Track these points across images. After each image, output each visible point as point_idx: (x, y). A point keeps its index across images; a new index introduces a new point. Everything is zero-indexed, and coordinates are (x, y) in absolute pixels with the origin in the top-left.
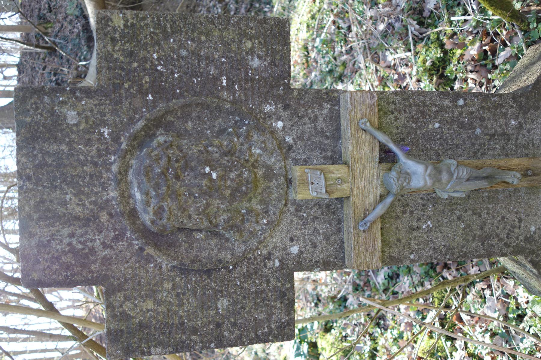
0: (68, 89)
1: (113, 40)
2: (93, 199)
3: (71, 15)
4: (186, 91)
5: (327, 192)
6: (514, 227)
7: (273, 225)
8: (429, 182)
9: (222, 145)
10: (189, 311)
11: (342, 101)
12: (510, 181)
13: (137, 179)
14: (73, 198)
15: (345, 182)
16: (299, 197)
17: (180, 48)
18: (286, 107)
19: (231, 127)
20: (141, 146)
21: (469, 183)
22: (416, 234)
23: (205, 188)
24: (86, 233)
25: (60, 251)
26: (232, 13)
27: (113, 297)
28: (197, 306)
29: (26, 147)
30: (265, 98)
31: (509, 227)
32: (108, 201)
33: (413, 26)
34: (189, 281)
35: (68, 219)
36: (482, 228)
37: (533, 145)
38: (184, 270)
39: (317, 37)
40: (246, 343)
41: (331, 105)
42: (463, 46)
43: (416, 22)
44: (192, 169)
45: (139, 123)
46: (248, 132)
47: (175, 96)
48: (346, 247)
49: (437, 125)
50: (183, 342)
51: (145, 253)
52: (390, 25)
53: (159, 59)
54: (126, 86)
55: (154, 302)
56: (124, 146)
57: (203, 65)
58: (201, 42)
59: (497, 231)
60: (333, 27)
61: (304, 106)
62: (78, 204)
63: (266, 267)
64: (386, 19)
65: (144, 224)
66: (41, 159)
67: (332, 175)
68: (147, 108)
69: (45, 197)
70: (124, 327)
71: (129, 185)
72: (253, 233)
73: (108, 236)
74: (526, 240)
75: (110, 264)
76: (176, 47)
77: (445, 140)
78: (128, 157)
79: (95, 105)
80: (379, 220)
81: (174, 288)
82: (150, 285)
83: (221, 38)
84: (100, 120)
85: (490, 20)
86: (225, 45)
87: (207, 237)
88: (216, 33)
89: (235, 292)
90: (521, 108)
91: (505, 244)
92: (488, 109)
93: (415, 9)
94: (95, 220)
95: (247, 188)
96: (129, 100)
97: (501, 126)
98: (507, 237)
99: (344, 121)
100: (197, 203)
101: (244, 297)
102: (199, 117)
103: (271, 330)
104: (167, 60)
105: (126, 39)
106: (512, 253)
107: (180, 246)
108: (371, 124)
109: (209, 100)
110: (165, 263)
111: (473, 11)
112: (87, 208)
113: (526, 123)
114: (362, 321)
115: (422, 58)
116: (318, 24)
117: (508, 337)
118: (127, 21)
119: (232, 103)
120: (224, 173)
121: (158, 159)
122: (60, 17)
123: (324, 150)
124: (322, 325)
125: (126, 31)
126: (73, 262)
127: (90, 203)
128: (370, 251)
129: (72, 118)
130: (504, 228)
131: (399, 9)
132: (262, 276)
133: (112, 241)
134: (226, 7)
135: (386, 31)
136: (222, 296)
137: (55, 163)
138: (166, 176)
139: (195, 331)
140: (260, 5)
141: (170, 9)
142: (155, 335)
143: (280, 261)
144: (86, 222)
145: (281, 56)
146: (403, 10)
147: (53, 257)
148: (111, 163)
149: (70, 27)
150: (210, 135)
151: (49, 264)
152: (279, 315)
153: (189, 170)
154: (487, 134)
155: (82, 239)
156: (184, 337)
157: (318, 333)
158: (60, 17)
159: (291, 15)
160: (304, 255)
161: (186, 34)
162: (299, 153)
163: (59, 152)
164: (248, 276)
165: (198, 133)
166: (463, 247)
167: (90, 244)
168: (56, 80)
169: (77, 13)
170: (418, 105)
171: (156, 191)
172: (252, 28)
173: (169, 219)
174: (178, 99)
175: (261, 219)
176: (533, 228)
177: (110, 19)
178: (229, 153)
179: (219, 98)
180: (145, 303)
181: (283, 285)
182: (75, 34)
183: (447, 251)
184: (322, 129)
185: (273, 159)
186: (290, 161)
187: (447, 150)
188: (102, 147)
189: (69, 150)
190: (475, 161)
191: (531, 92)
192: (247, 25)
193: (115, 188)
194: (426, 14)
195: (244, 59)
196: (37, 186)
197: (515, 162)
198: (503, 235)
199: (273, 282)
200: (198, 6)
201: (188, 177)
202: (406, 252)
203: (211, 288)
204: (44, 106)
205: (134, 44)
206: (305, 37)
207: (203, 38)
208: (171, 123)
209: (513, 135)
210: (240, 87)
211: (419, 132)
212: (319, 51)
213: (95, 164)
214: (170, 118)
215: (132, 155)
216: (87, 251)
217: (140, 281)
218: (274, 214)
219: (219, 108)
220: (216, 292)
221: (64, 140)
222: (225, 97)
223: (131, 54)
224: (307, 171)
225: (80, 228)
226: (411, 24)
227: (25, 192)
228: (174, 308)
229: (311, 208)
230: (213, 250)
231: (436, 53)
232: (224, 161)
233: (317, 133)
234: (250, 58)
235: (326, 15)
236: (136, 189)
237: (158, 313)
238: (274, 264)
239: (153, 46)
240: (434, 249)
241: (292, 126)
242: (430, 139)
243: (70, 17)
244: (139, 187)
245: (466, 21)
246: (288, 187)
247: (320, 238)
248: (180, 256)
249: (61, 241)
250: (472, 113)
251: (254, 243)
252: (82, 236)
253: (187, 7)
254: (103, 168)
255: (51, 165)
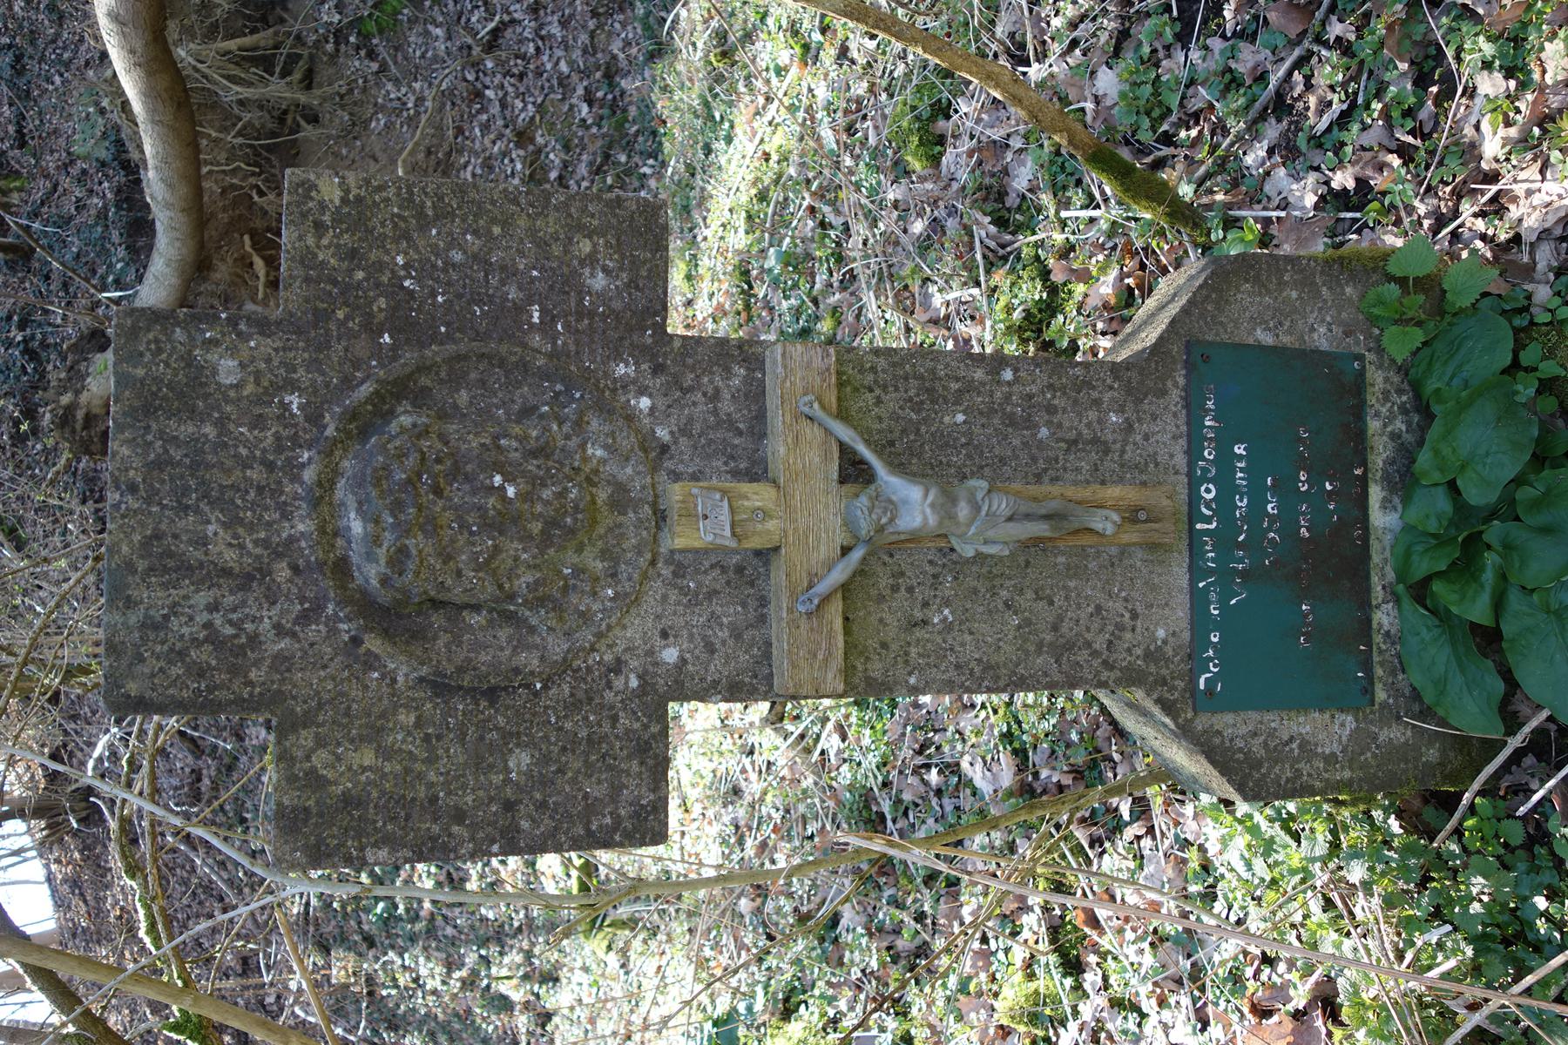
0: (223, 316)
1: (319, 227)
2: (262, 535)
3: (85, 158)
4: (459, 330)
5: (734, 534)
6: (1120, 627)
7: (628, 602)
8: (932, 520)
9: (526, 437)
10: (448, 773)
11: (768, 360)
12: (1098, 526)
13: (355, 494)
14: (221, 532)
15: (771, 517)
16: (680, 543)
17: (450, 246)
18: (658, 369)
19: (547, 404)
20: (364, 434)
21: (1011, 524)
22: (919, 633)
23: (492, 512)
24: (244, 603)
25: (187, 637)
26: (553, 175)
27: (292, 738)
28: (466, 763)
29: (132, 426)
30: (616, 350)
31: (1111, 628)
32: (292, 540)
33: (984, 227)
34: (450, 712)
35: (209, 573)
36: (1055, 628)
37: (1157, 465)
38: (440, 687)
39: (771, 245)
40: (566, 847)
41: (748, 369)
42: (1085, 276)
43: (988, 219)
44: (468, 478)
45: (363, 388)
46: (581, 414)
47: (435, 338)
48: (775, 652)
49: (960, 418)
50: (434, 839)
51: (362, 650)
52: (936, 225)
53: (406, 266)
54: (340, 314)
55: (377, 751)
56: (330, 431)
57: (494, 282)
58: (490, 237)
59: (1088, 636)
60: (811, 223)
61: (693, 369)
62: (230, 545)
63: (610, 688)
64: (928, 210)
65: (364, 592)
66: (160, 451)
67: (746, 503)
68: (379, 359)
69: (163, 527)
70: (311, 803)
71: (337, 509)
72: (585, 616)
73: (288, 611)
74: (1148, 656)
75: (288, 670)
76: (441, 244)
77: (976, 447)
78: (338, 453)
79: (276, 350)
80: (839, 595)
81: (419, 724)
82: (369, 715)
83: (532, 232)
84: (284, 380)
85: (1136, 220)
86: (538, 246)
87: (491, 622)
88: (522, 222)
89: (546, 737)
90: (1129, 392)
91: (1105, 663)
92: (1063, 389)
93: (989, 188)
94: (264, 578)
95: (576, 520)
96: (344, 343)
97: (1089, 425)
98: (1108, 648)
99: (772, 401)
100: (474, 544)
101: (564, 749)
102: (483, 383)
103: (618, 821)
104: (424, 270)
105: (344, 226)
106: (1118, 682)
107: (435, 638)
108: (823, 407)
109: (504, 349)
110: (403, 670)
111: (1106, 200)
112: (249, 554)
113: (1139, 420)
114: (874, 964)
115: (1002, 303)
116: (774, 213)
117: (1189, 941)
118: (347, 191)
119: (550, 356)
120: (529, 488)
121: (401, 455)
122: (50, 162)
123: (732, 457)
124: (776, 1000)
125: (346, 210)
126: (214, 663)
127: (256, 542)
128: (820, 657)
129: (229, 373)
130: (1101, 631)
131: (955, 186)
132: (602, 706)
133: (296, 622)
134: (537, 159)
135: (929, 237)
136: (518, 745)
137: (188, 461)
138: (415, 488)
139: (459, 816)
140: (629, 157)
141: (379, 154)
142: (375, 822)
143: (639, 677)
144: (245, 581)
145: (650, 271)
146: (964, 188)
147: (172, 650)
148: (303, 465)
149: (79, 192)
150: (503, 418)
151: (162, 664)
152: (636, 790)
153: (461, 478)
154: (1063, 440)
155: (234, 616)
156: (436, 829)
157: (764, 1024)
158: (50, 162)
159: (709, 188)
160: (690, 667)
161: (464, 220)
162: (682, 461)
163: (197, 440)
164: (574, 705)
165: (480, 412)
166: (1017, 665)
167: (249, 626)
168: (25, 341)
169: (103, 154)
170: (922, 378)
171: (395, 517)
172: (593, 216)
173: (417, 574)
174: (442, 344)
175: (603, 588)
176: (1161, 633)
177: (314, 187)
178: (542, 451)
179: (524, 346)
180: (358, 755)
181: (646, 727)
182: (93, 212)
183: (984, 670)
184: (729, 415)
185: (629, 470)
186: (662, 476)
187: (982, 467)
188: (285, 433)
189: (219, 436)
190: (1034, 489)
191: (1147, 359)
192: (584, 210)
193: (309, 515)
194: (1013, 200)
195: (575, 274)
196: (149, 504)
197: (1113, 492)
198: (1100, 643)
199: (624, 721)
200: (460, 152)
201: (458, 493)
202: (901, 671)
203: (497, 728)
204: (174, 348)
205: (359, 235)
206: (741, 246)
207: (497, 230)
208: (426, 391)
209: (1114, 442)
210: (567, 326)
211: (923, 429)
212: (775, 283)
213: (270, 466)
214: (424, 381)
215: (345, 450)
216: (244, 640)
217: (349, 708)
218: (630, 579)
219: (525, 365)
220: (506, 736)
221: (209, 415)
222: (536, 345)
223: (353, 254)
224: (695, 491)
225: (231, 592)
226: (978, 223)
227: (123, 517)
228: (418, 766)
229: (705, 572)
230: (502, 649)
231: (1031, 292)
232: (532, 466)
233: (719, 423)
234: (587, 271)
235: (794, 192)
236: (352, 515)
237: (384, 776)
238: (627, 683)
239: (396, 241)
240: (958, 667)
241: (669, 406)
242: (947, 444)
243: (80, 165)
244: (359, 511)
245: (1092, 220)
246: (658, 527)
247: (724, 634)
248: (434, 657)
249: (191, 619)
250: (1030, 397)
251: (586, 636)
252: (234, 610)
253: (429, 153)
254: (285, 473)
255: (179, 463)
